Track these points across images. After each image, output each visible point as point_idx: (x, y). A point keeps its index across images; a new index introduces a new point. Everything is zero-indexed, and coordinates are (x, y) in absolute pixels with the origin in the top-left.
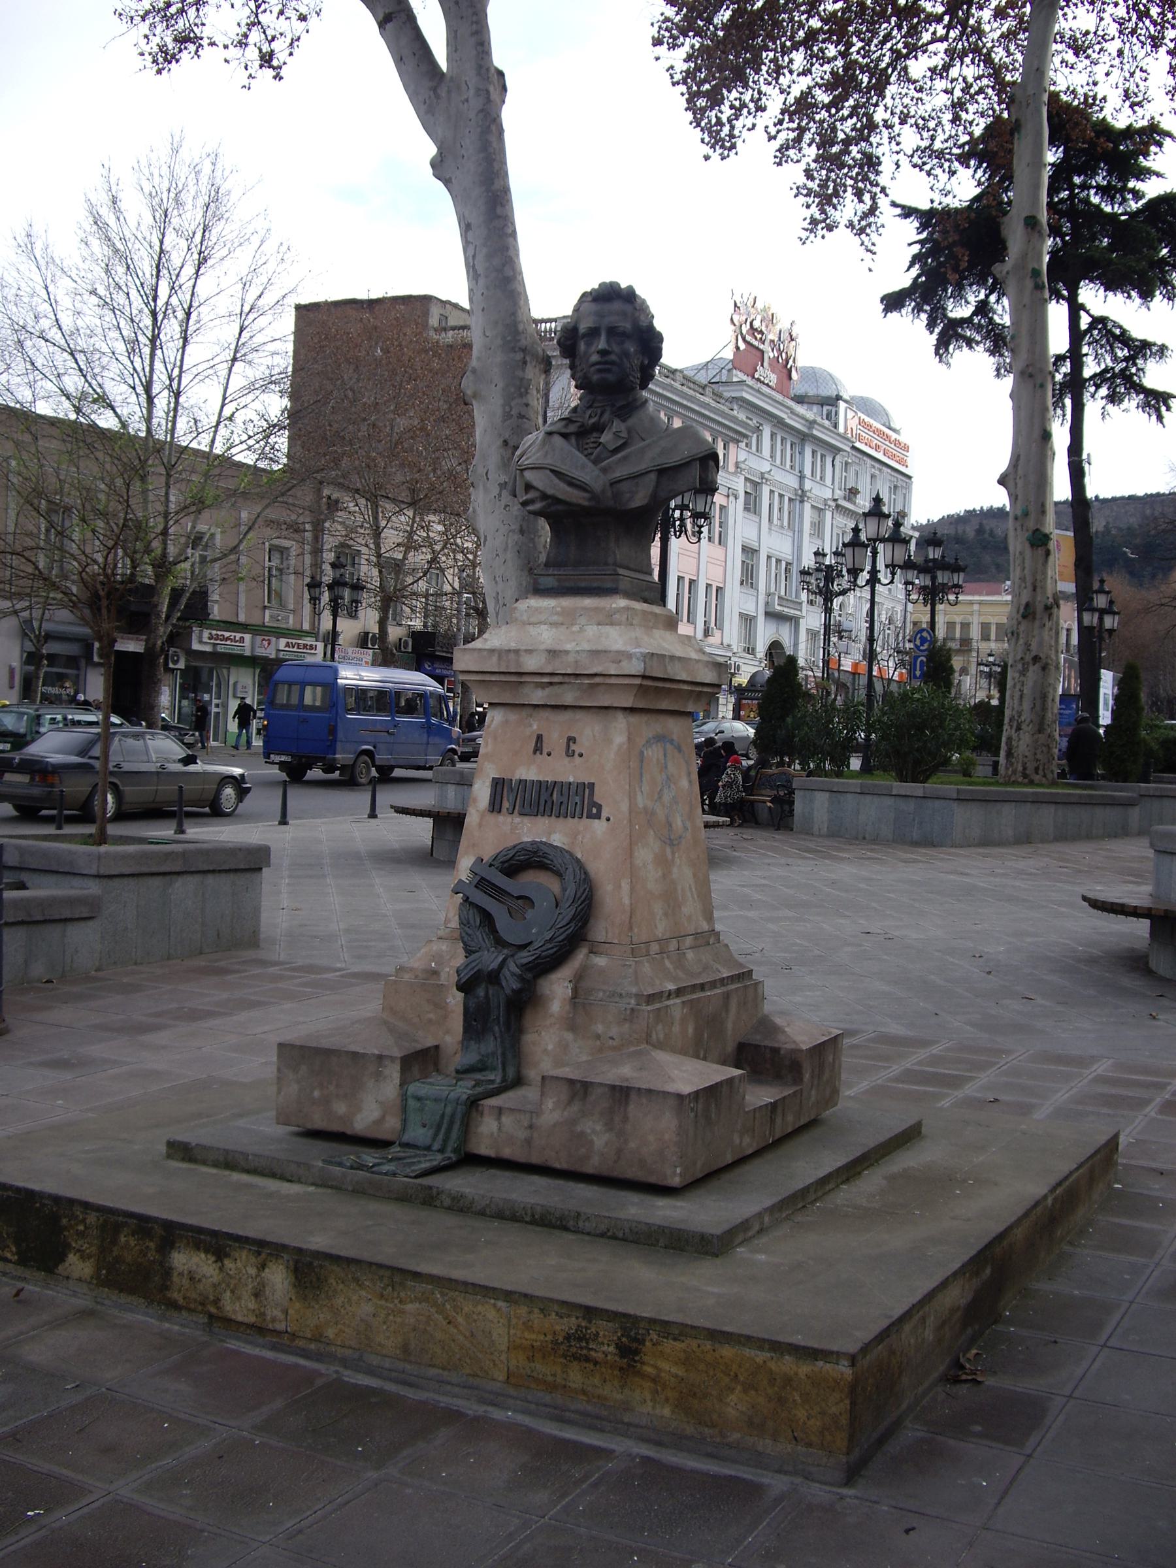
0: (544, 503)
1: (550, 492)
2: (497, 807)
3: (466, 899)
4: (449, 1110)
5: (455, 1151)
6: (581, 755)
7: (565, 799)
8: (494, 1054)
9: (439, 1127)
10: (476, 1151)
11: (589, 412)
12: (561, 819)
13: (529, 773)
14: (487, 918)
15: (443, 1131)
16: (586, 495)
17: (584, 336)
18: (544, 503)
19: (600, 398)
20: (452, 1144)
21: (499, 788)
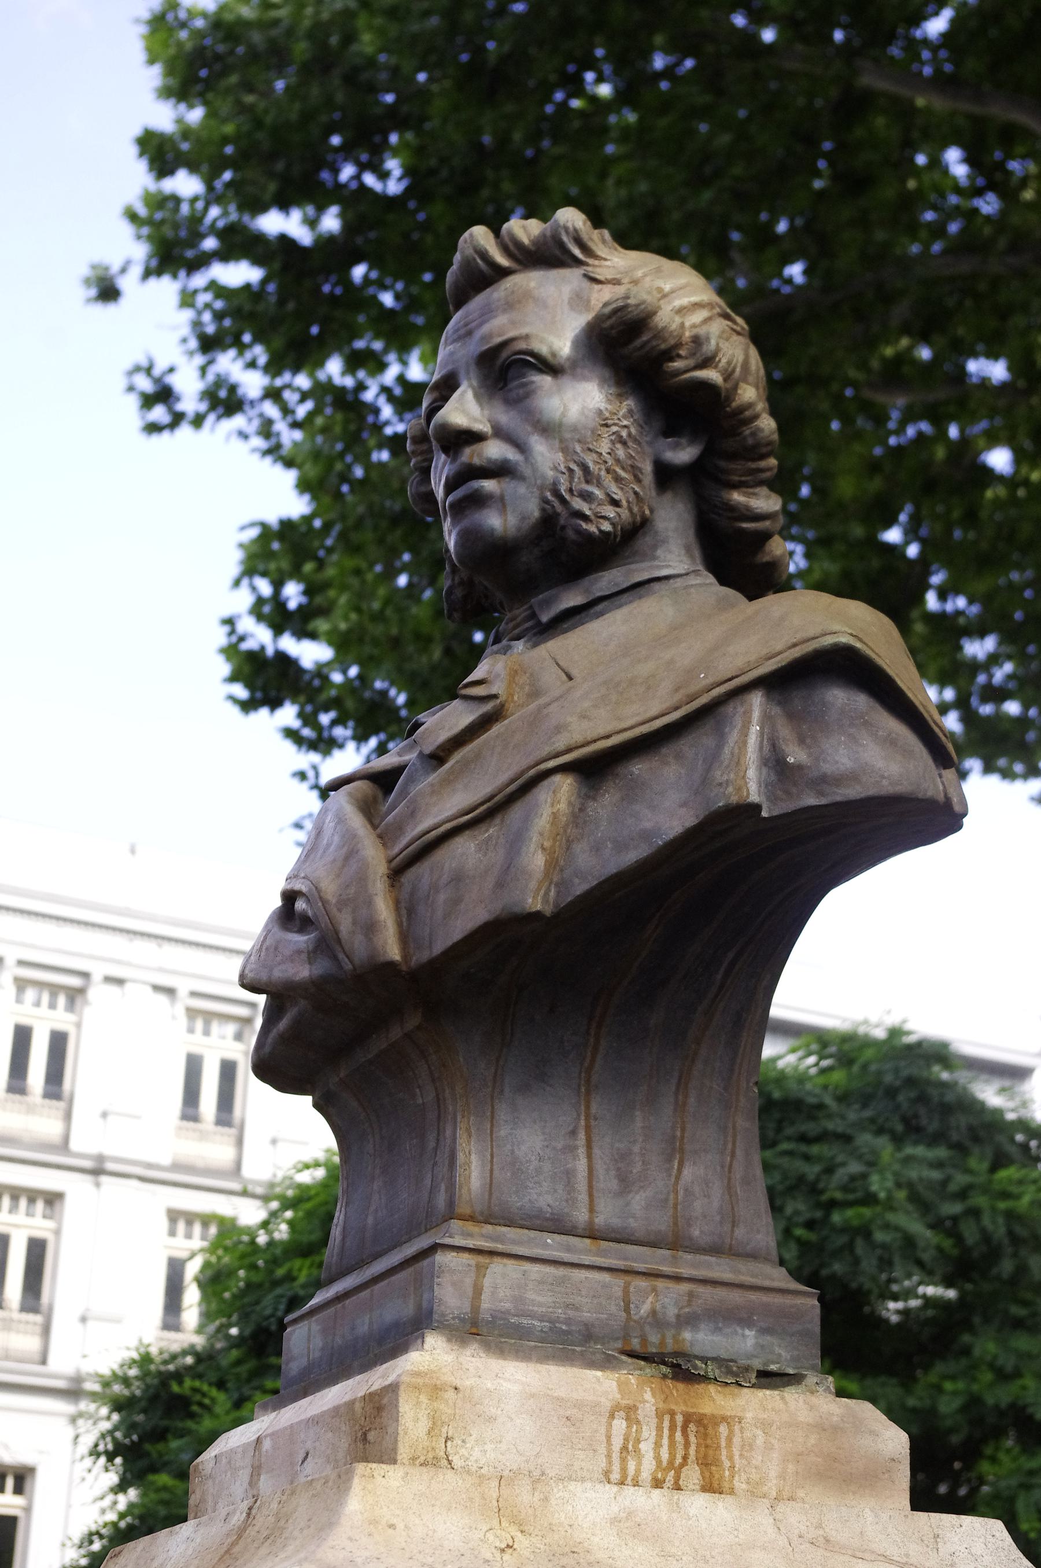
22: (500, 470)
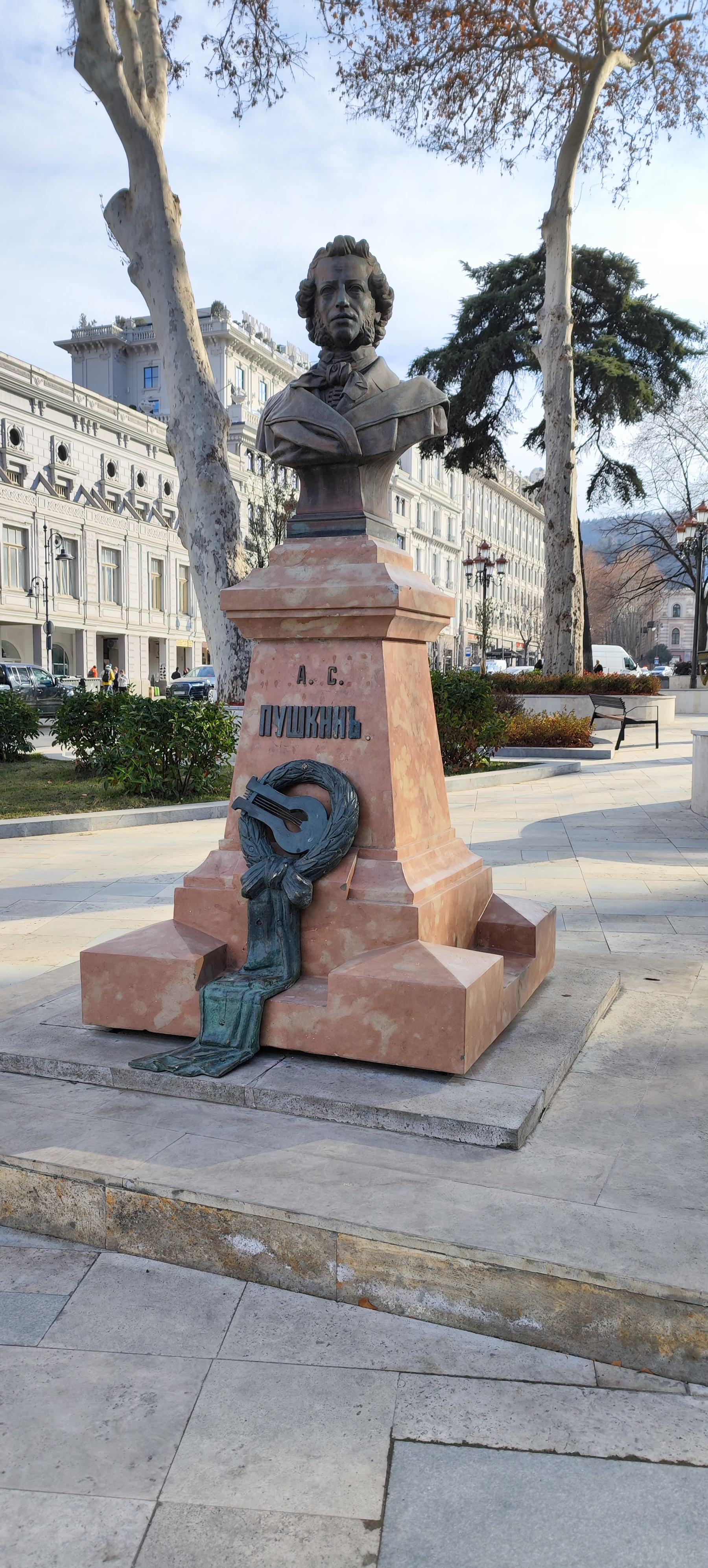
0: (294, 454)
1: (299, 442)
2: (267, 731)
3: (246, 814)
4: (245, 1009)
5: (252, 1046)
6: (342, 683)
7: (328, 721)
8: (279, 951)
9: (236, 1027)
10: (271, 1044)
11: (329, 367)
12: (326, 740)
13: (294, 699)
14: (265, 831)
15: (240, 1029)
16: (335, 443)
17: (323, 290)
18: (294, 454)
19: (339, 353)
20: (250, 1039)
21: (269, 712)
22: (354, 318)
